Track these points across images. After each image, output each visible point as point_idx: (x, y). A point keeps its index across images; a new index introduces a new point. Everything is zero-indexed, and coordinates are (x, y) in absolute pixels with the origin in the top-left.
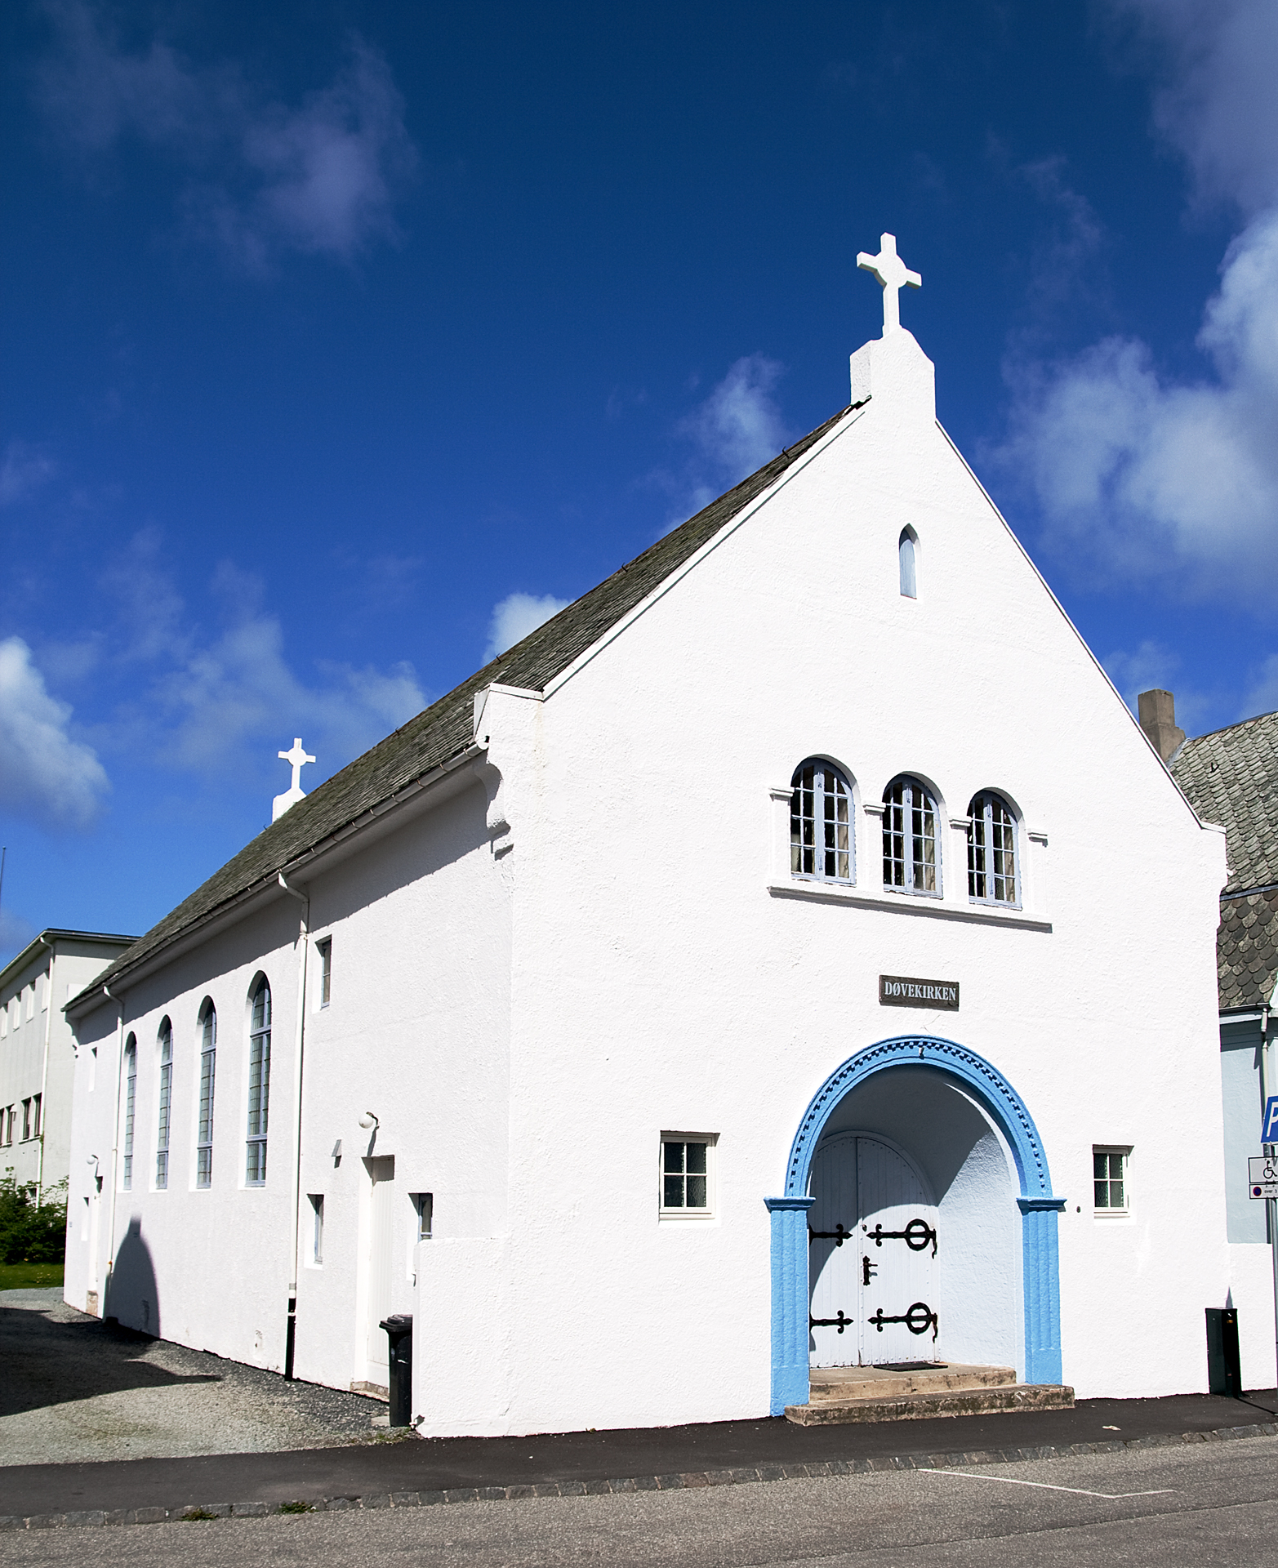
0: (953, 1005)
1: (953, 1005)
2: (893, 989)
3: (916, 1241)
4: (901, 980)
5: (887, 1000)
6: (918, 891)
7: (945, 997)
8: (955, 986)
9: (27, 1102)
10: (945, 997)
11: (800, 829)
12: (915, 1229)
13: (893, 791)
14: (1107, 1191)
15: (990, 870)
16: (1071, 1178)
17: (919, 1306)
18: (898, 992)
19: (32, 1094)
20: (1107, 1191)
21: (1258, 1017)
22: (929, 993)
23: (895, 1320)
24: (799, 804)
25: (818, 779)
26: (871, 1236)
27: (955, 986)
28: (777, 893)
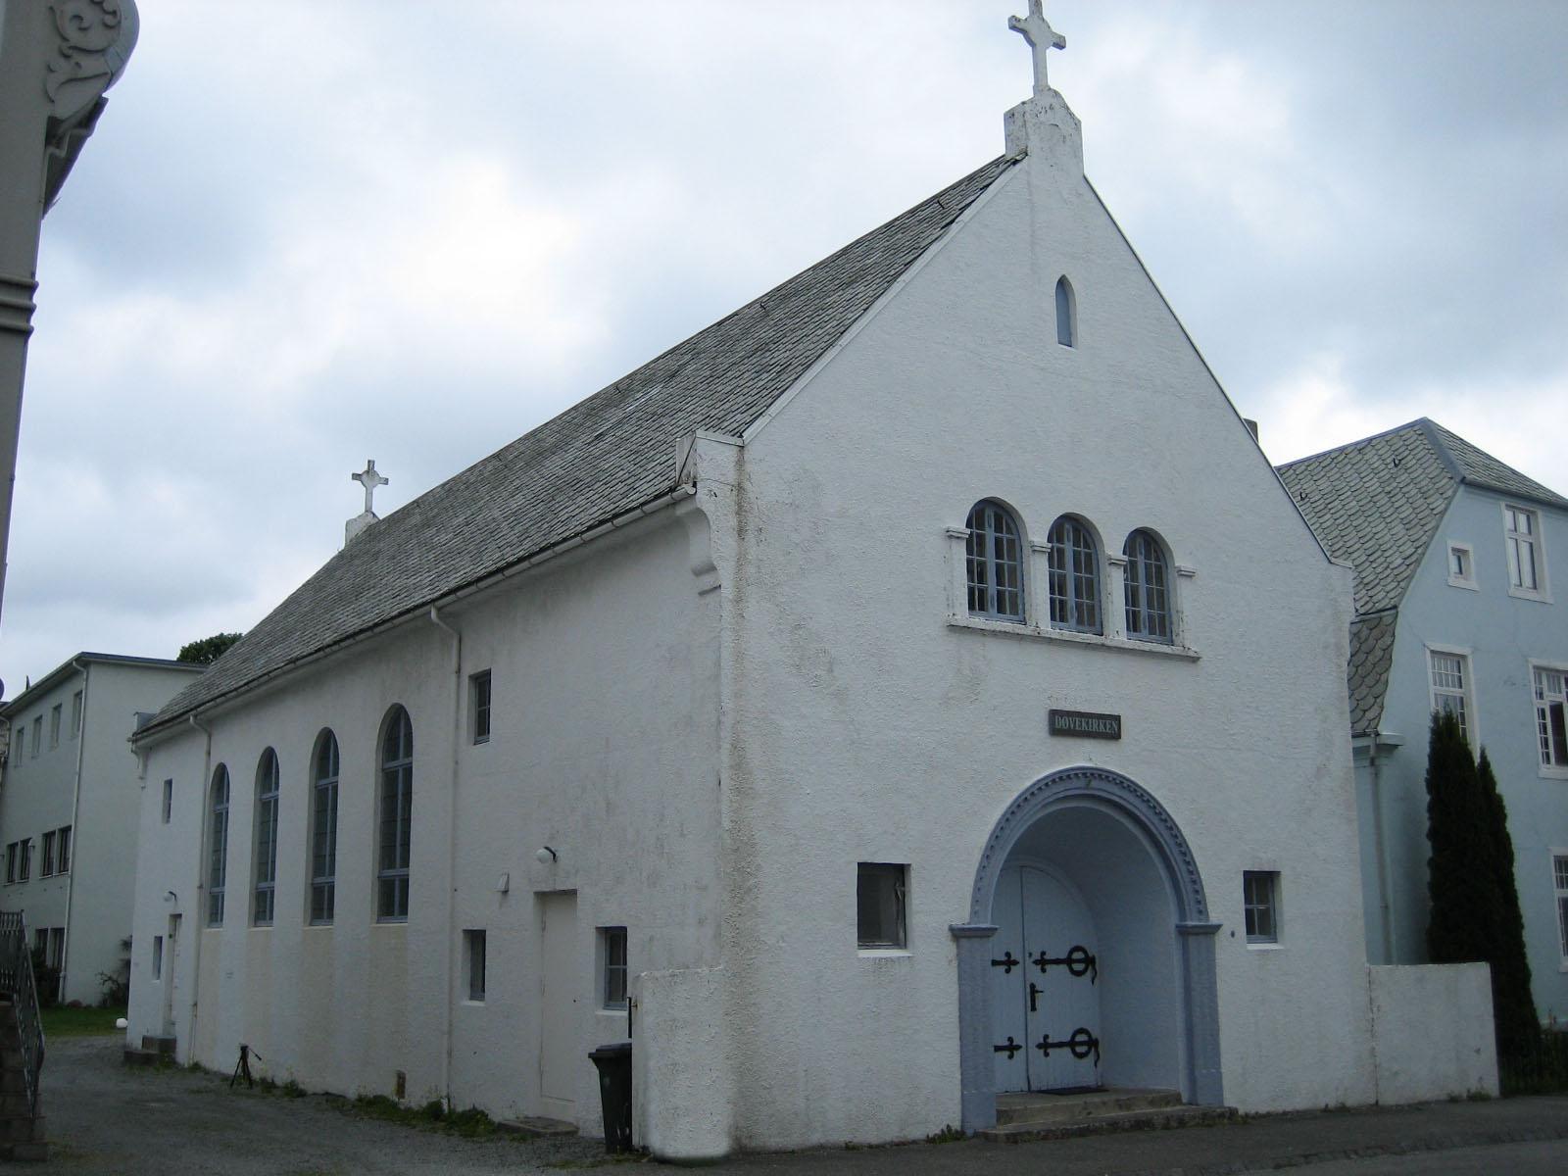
0: (1115, 736)
1: (1115, 736)
2: (1062, 723)
3: (1080, 1049)
4: (1069, 714)
5: (1056, 731)
6: (1081, 628)
7: (1107, 728)
8: (1117, 718)
9: (48, 837)
10: (1107, 728)
11: (976, 572)
12: (1080, 1038)
13: (1057, 532)
14: (1261, 921)
15: (1153, 616)
16: (1226, 904)
17: (1081, 1031)
18: (1066, 725)
19: (55, 825)
20: (1261, 921)
21: (1007, 594)
22: (1095, 726)
23: (1060, 1045)
24: (975, 544)
25: (992, 521)
26: (1036, 962)
27: (1117, 718)
28: (953, 628)
